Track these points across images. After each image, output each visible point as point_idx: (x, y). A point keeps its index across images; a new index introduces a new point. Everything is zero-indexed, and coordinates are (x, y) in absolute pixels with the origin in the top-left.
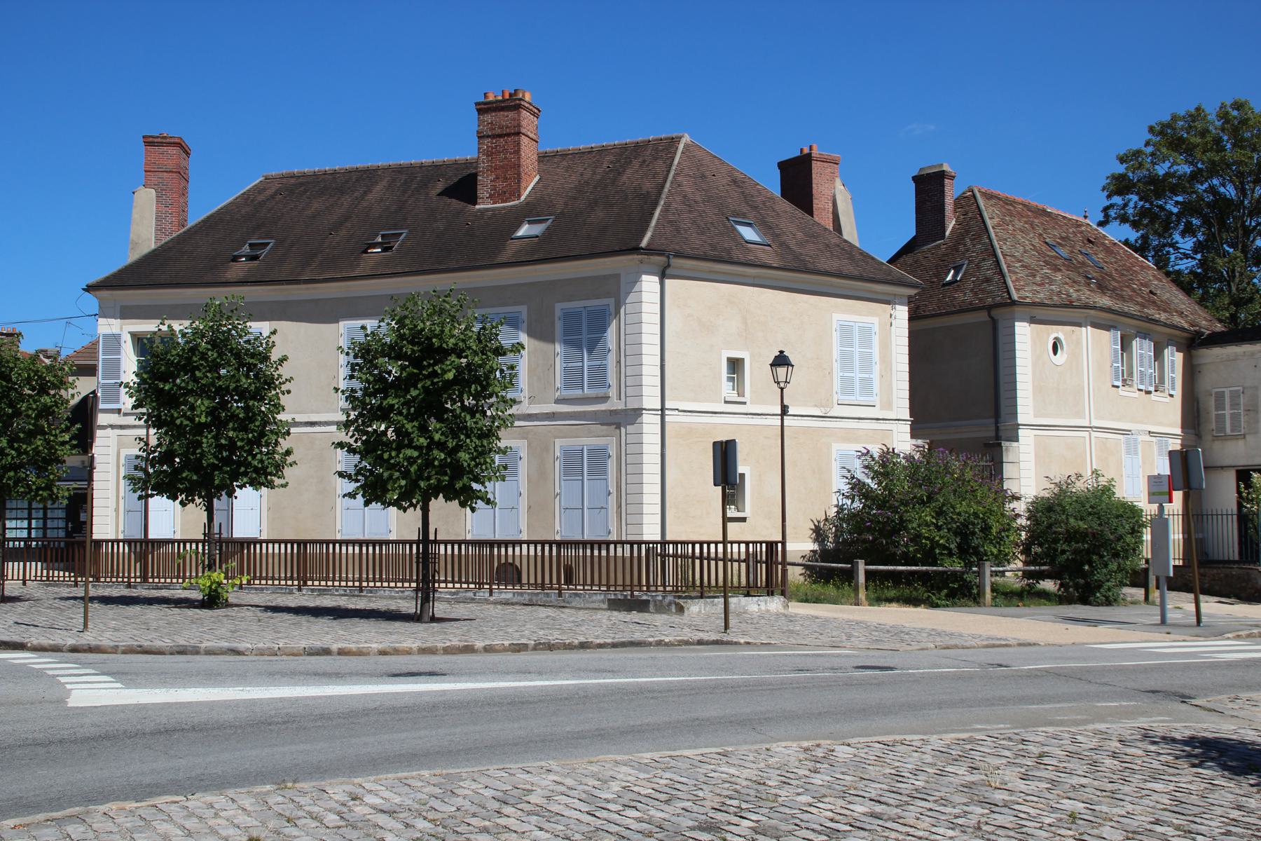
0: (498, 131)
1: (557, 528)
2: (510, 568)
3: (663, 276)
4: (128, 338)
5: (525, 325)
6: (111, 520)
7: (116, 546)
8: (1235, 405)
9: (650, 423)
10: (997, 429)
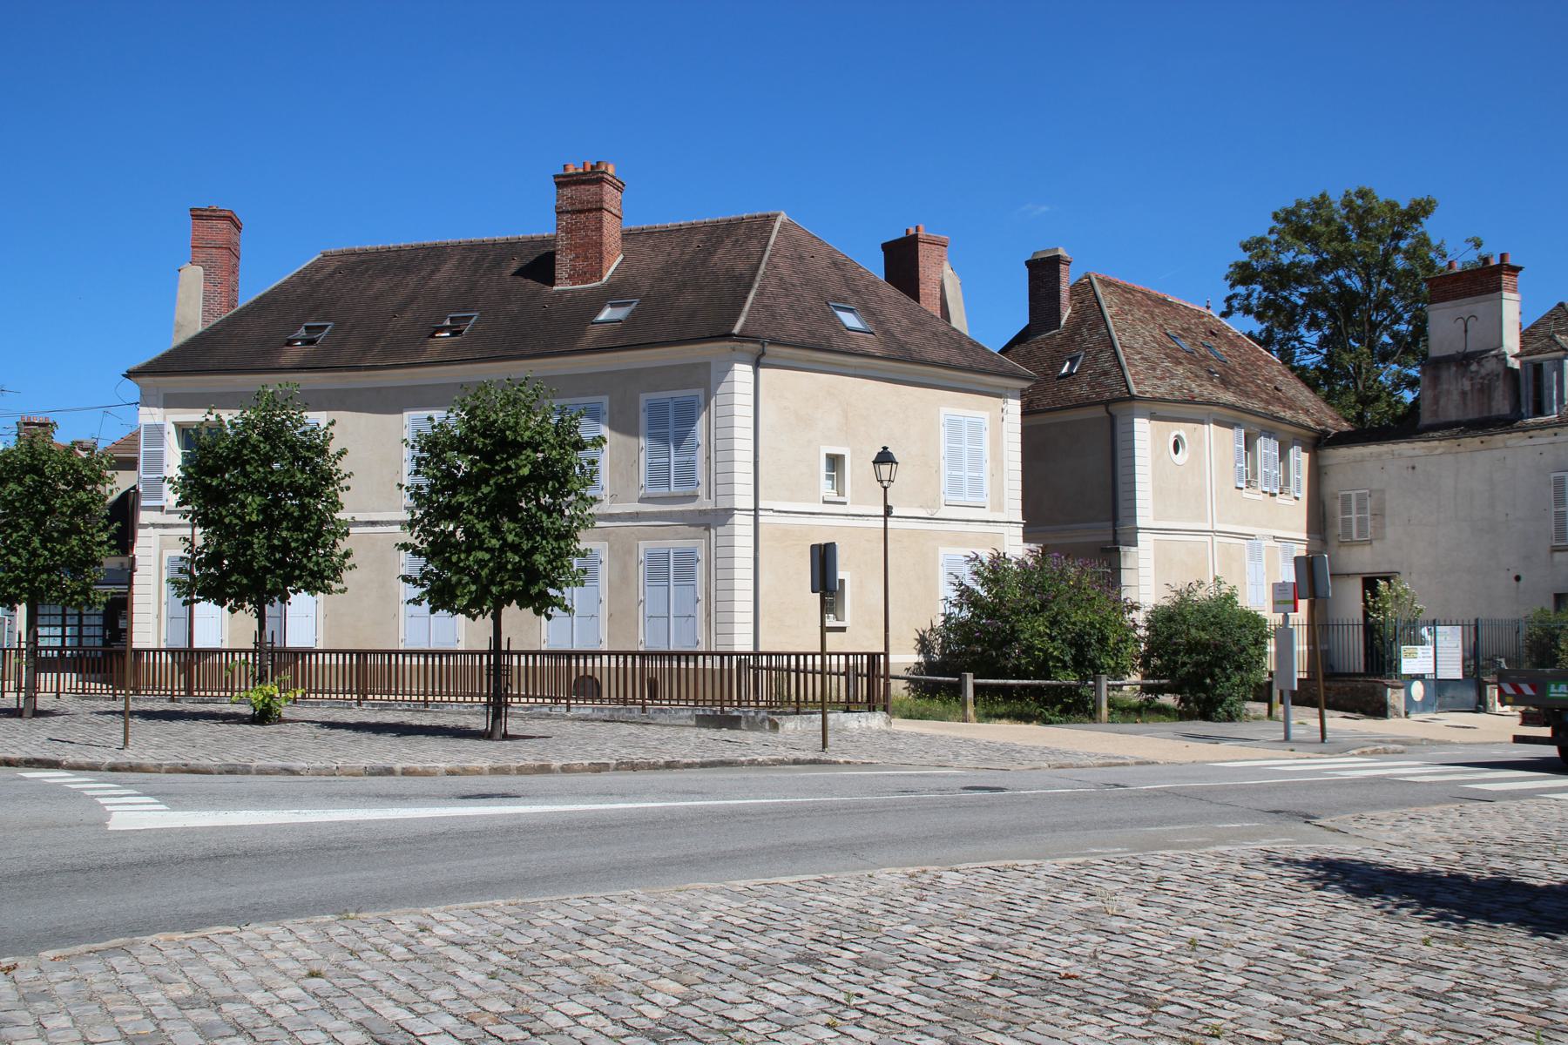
0: (578, 207)
1: (641, 638)
2: (589, 682)
3: (757, 365)
4: (172, 429)
5: (606, 417)
6: (152, 628)
8: (1361, 509)
10: (1115, 532)
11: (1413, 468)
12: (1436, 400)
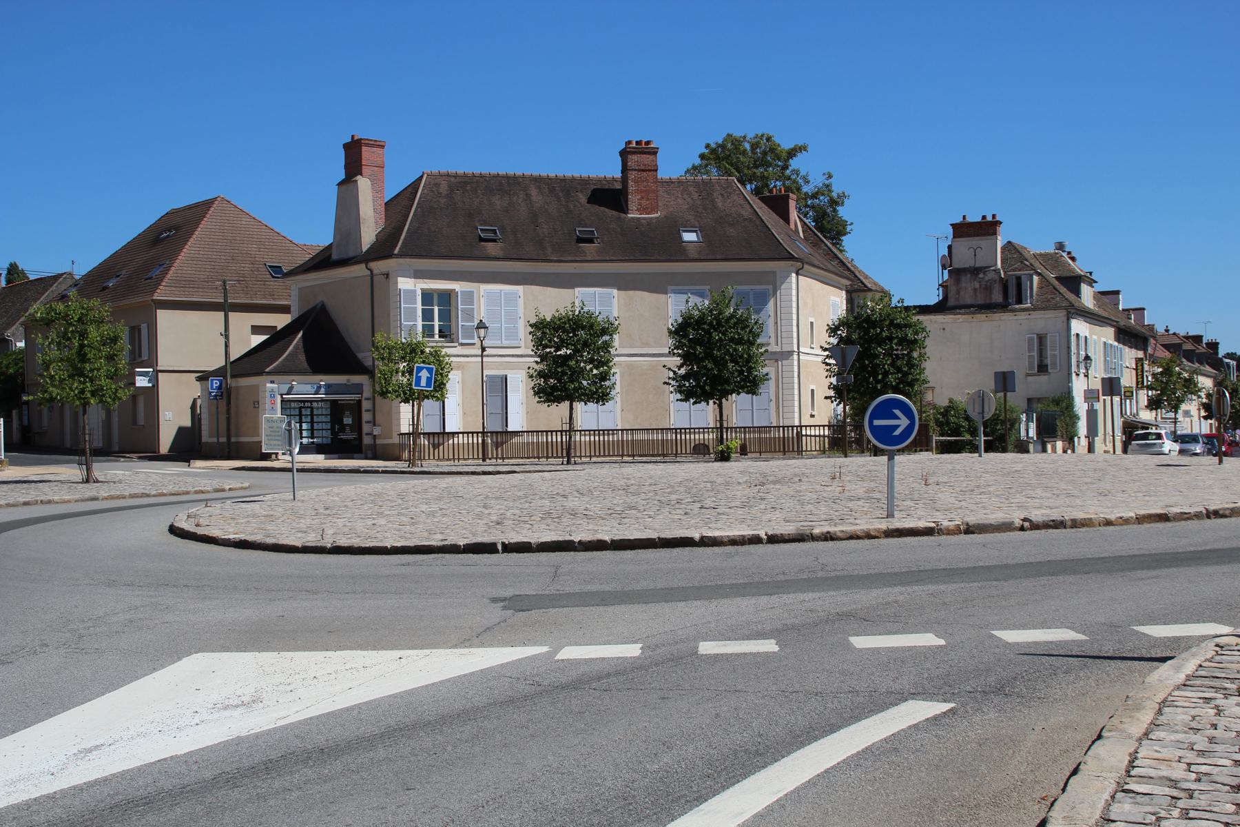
0: (643, 168)
1: (735, 421)
3: (797, 274)
7: (790, 431)
9: (795, 357)
11: (944, 329)
12: (958, 292)
